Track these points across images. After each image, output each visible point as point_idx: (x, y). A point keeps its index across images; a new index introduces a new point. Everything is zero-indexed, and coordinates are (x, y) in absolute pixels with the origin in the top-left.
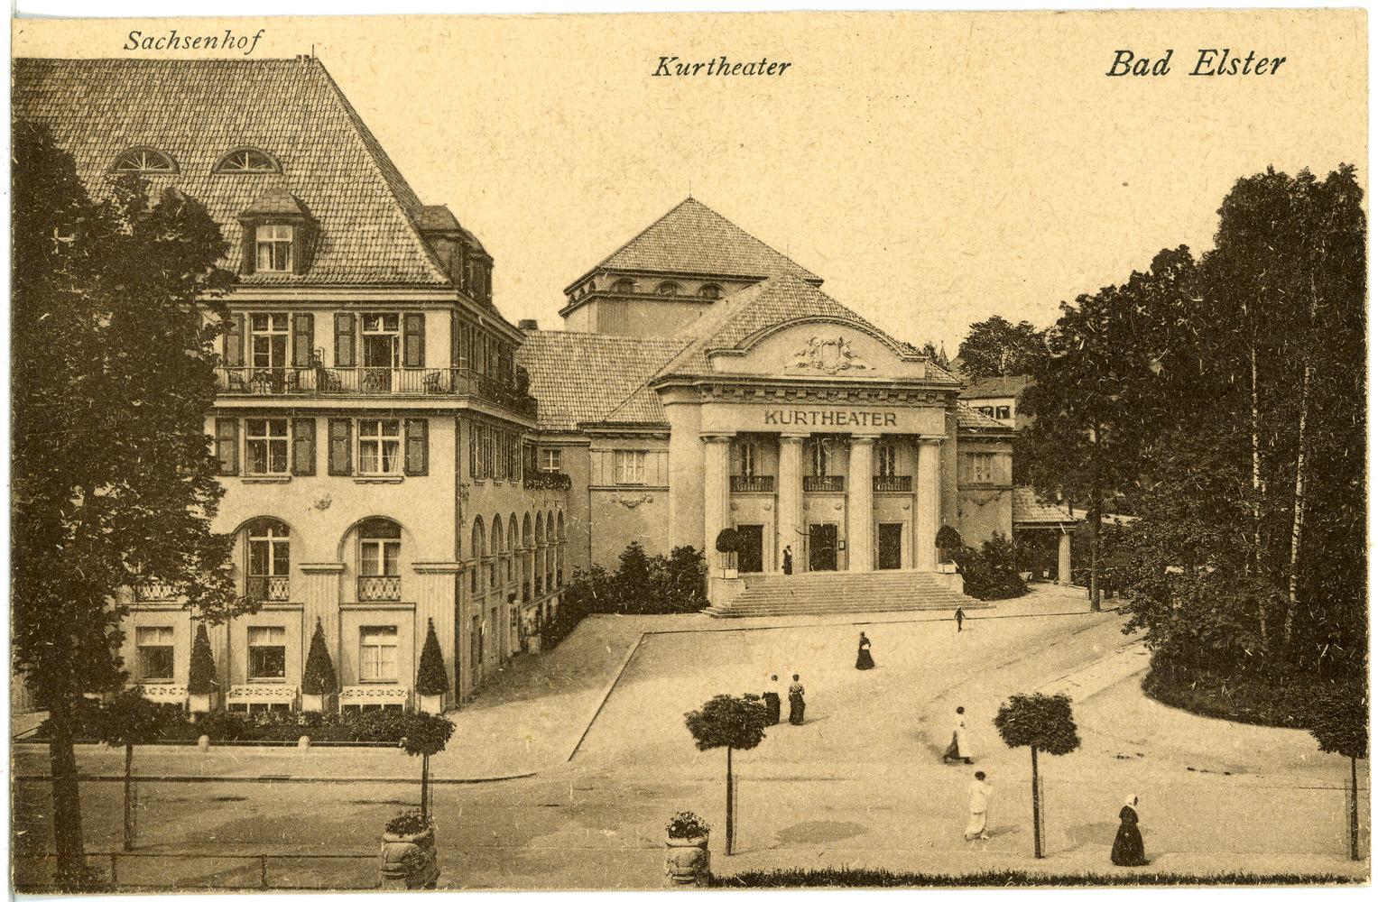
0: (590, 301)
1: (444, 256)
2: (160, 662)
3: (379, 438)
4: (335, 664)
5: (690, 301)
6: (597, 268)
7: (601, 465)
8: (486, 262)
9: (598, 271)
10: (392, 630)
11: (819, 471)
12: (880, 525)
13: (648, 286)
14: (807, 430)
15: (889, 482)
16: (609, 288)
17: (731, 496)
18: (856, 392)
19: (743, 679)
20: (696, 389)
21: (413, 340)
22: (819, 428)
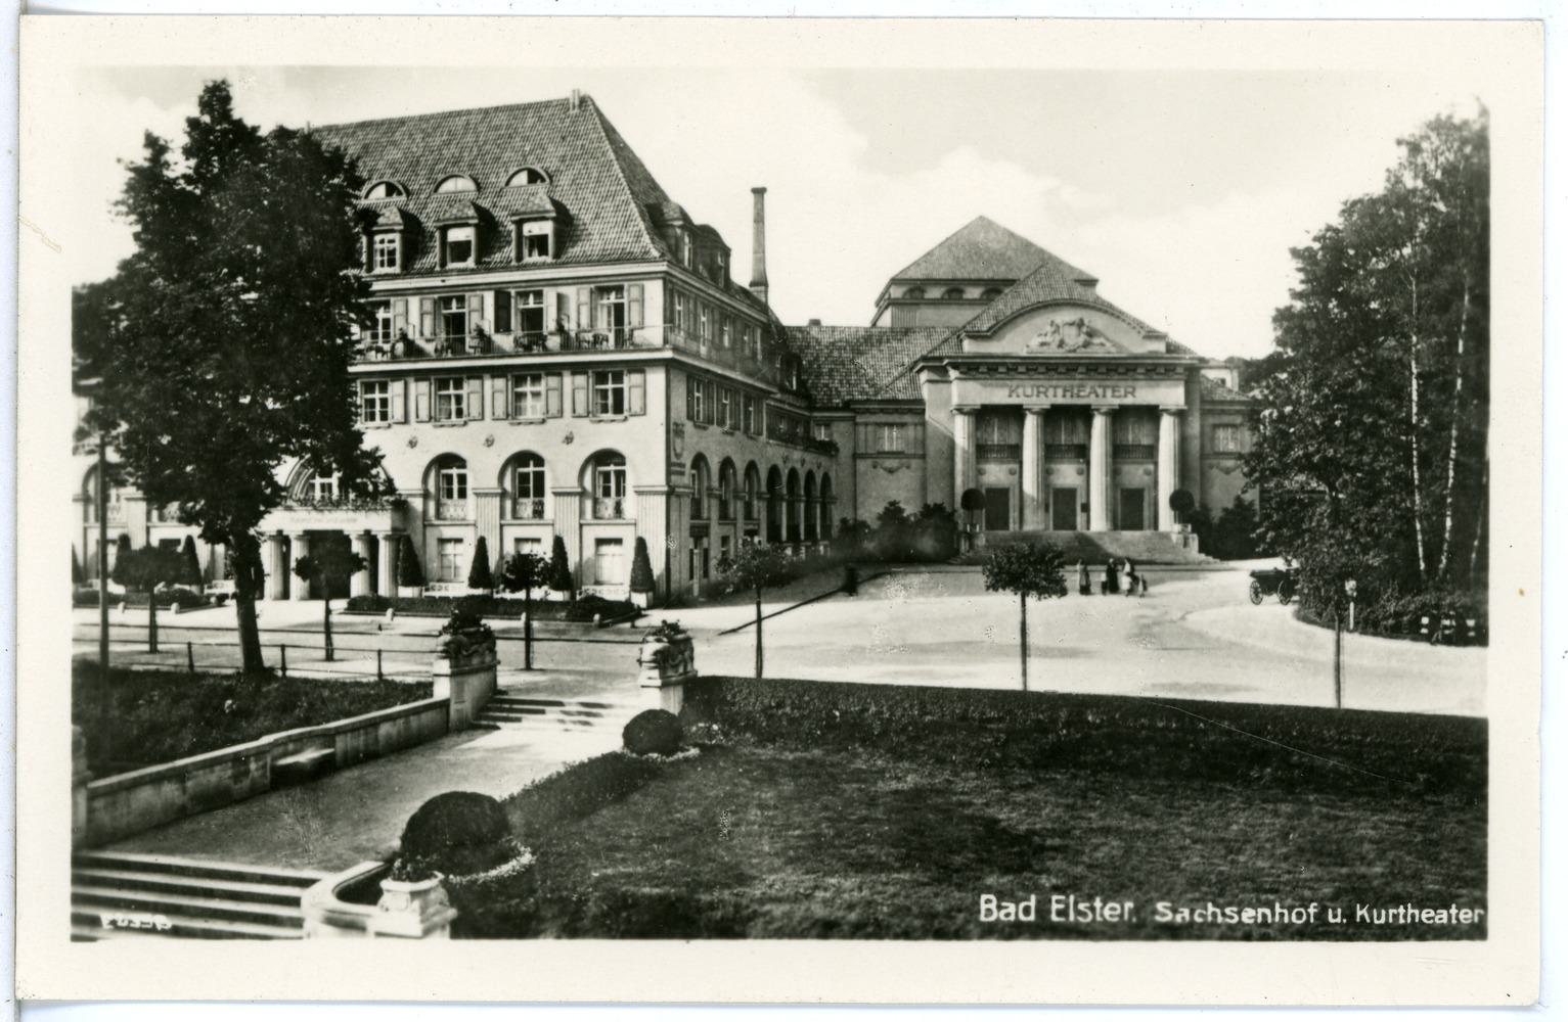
5: (936, 282)
12: (1123, 491)
13: (935, 293)
14: (1045, 402)
17: (978, 462)
20: (936, 365)
22: (1060, 400)
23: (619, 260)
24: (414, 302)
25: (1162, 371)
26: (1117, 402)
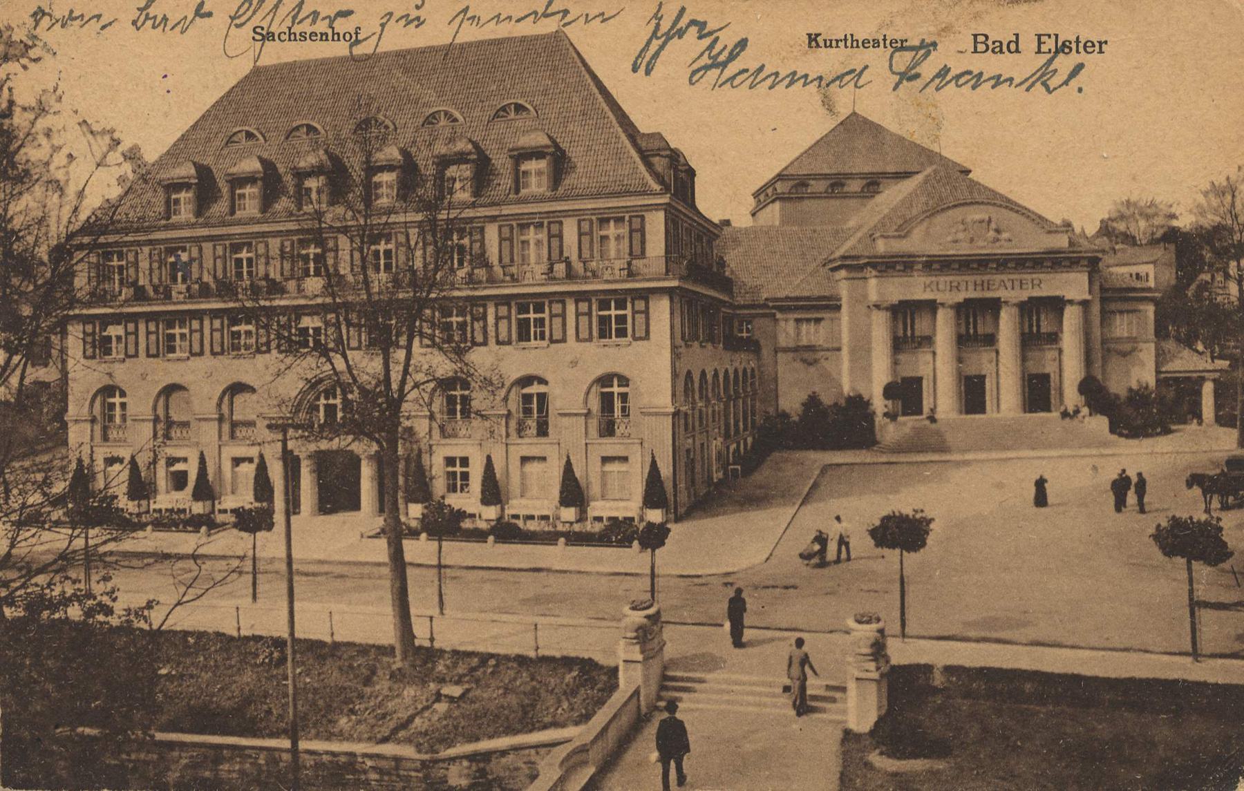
0: (773, 201)
1: (659, 169)
2: (458, 482)
3: (532, 316)
4: (583, 483)
5: (854, 196)
6: (779, 175)
7: (787, 331)
8: (691, 173)
9: (780, 177)
10: (625, 459)
11: (909, 333)
15: (1035, 339)
16: (790, 188)
18: (1005, 263)
19: (905, 503)
20: (854, 265)
21: (637, 236)
22: (972, 294)
23: (628, 193)
24: (207, 247)
25: (975, 266)
26: (1024, 296)
